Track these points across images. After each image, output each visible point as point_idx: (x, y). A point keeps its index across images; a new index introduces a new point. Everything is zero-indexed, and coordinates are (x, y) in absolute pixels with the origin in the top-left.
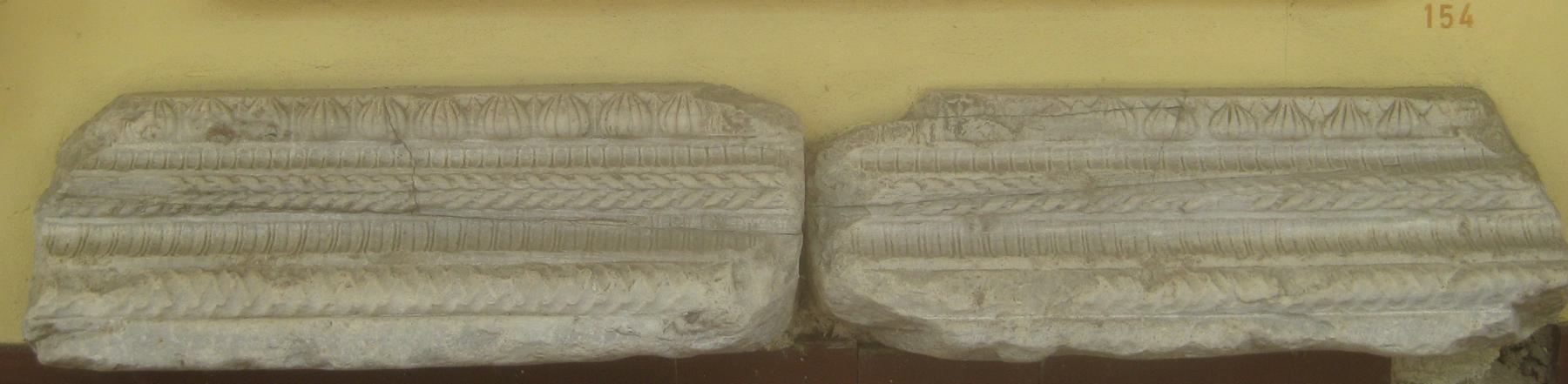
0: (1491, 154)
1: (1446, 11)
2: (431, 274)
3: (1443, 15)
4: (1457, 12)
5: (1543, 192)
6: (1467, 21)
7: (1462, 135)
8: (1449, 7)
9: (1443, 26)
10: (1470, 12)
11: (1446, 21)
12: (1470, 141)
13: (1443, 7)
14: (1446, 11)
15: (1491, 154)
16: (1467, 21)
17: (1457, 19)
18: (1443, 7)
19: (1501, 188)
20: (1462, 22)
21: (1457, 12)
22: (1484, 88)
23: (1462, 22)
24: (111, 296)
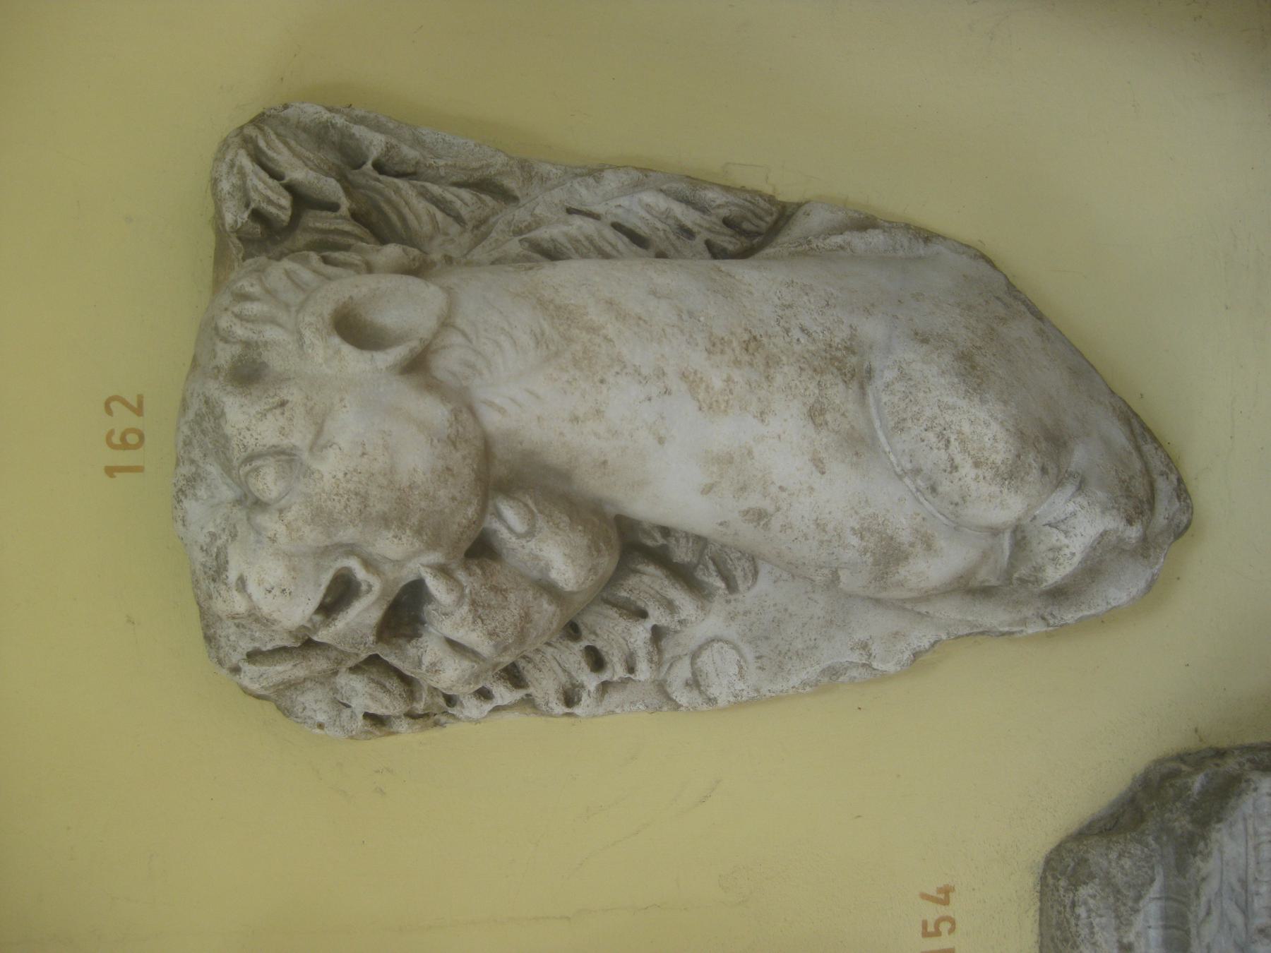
0: (1157, 886)
1: (931, 929)
2: (403, 219)
3: (937, 933)
4: (932, 912)
5: (1123, 551)
6: (944, 895)
7: (1130, 937)
8: (925, 924)
9: (952, 931)
10: (932, 891)
11: (945, 927)
12: (1139, 922)
13: (926, 934)
14: (931, 929)
15: (1157, 886)
16: (944, 895)
17: (943, 911)
18: (926, 934)
19: (1219, 893)
20: (946, 902)
21: (932, 912)
22: (1040, 859)
23: (946, 902)
24: (303, 331)
